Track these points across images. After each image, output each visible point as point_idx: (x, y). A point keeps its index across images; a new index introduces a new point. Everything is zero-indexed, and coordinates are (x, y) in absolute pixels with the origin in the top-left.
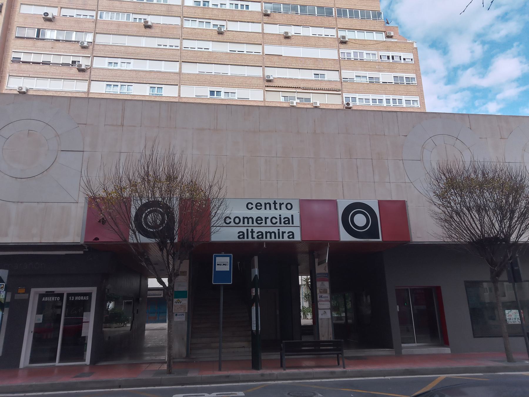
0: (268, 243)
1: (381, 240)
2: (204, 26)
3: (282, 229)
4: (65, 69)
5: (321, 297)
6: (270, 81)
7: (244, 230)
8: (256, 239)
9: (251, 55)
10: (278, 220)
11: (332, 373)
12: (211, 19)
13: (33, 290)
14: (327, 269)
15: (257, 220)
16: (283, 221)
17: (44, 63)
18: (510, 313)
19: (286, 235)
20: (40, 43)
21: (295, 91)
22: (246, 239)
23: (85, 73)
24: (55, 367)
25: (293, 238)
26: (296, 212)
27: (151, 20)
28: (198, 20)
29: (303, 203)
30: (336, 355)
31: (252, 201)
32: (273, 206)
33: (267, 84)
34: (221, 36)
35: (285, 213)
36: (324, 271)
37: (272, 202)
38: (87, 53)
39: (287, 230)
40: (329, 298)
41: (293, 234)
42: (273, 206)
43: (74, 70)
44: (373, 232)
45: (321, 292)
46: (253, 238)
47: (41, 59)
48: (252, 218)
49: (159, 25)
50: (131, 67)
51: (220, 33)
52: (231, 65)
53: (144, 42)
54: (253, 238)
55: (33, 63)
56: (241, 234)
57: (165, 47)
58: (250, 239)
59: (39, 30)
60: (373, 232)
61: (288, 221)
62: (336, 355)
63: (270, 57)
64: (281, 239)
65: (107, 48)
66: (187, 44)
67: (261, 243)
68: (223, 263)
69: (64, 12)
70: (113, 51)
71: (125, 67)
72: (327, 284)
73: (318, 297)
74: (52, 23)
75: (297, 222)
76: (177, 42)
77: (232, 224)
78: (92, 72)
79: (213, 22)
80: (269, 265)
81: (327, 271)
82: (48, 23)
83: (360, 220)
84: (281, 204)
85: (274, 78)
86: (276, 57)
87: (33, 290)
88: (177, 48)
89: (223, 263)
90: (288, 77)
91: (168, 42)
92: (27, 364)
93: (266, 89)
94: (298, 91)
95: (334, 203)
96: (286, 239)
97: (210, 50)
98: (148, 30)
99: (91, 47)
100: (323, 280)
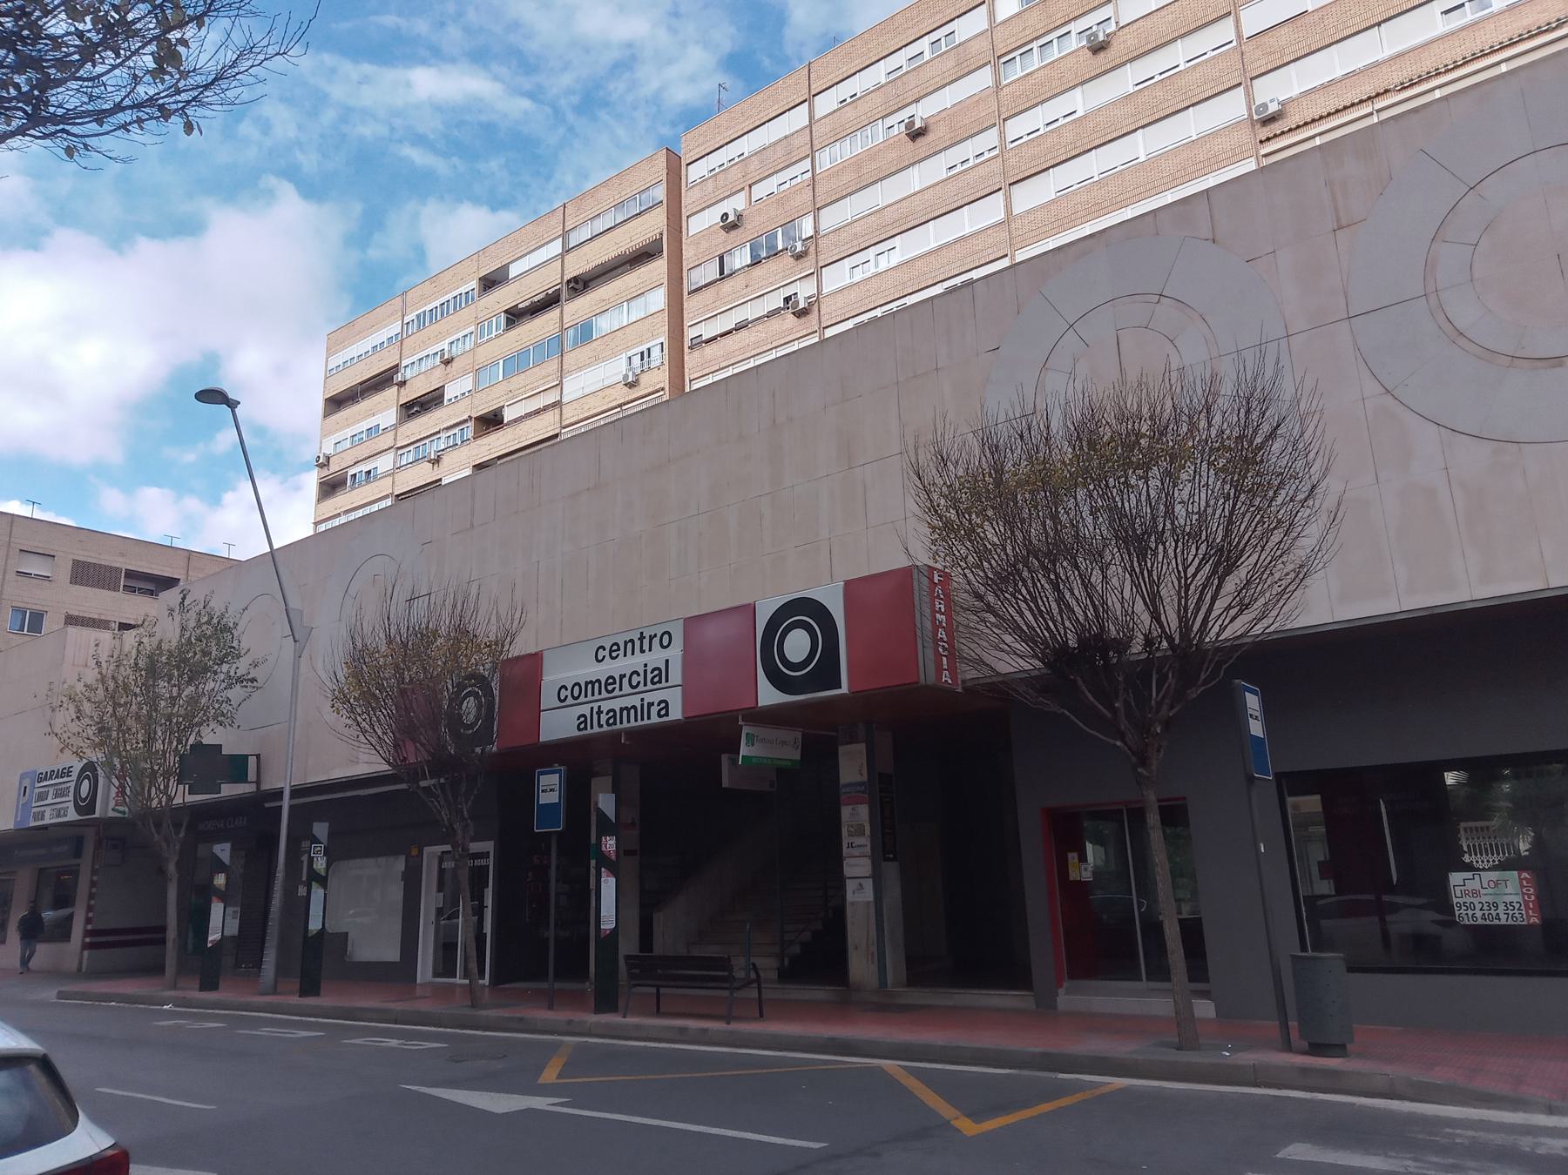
0: (630, 733)
1: (844, 689)
2: (1055, 53)
3: (649, 698)
4: (775, 324)
5: (850, 845)
6: (1272, 119)
7: (585, 710)
8: (605, 728)
9: (1206, 61)
10: (641, 679)
11: (683, 1030)
12: (1069, 22)
13: (427, 850)
14: (865, 772)
15: (607, 684)
16: (649, 676)
17: (739, 327)
18: (1470, 885)
19: (654, 710)
20: (727, 286)
21: (1369, 110)
22: (589, 731)
23: (809, 317)
24: (455, 985)
25: (667, 714)
26: (675, 653)
27: (922, 111)
28: (1035, 45)
29: (691, 623)
30: (654, 990)
31: (602, 646)
32: (637, 643)
33: (1264, 133)
34: (1102, 55)
35: (656, 657)
36: (859, 779)
37: (636, 637)
38: (808, 266)
39: (655, 697)
40: (868, 850)
41: (667, 707)
42: (637, 643)
43: (790, 318)
44: (825, 672)
45: (850, 835)
46: (600, 726)
47: (728, 322)
48: (599, 681)
49: (944, 115)
50: (895, 259)
51: (1098, 48)
52: (1143, 127)
53: (932, 171)
54: (600, 726)
55: (722, 335)
56: (583, 721)
57: (966, 166)
58: (596, 729)
59: (721, 258)
60: (825, 672)
61: (659, 676)
62: (654, 990)
63: (1265, 39)
64: (646, 722)
65: (844, 235)
66: (1018, 128)
67: (618, 733)
68: (550, 788)
69: (760, 191)
70: (856, 236)
71: (884, 264)
72: (864, 811)
73: (845, 846)
74: (740, 230)
75: (676, 675)
76: (990, 138)
77: (570, 701)
78: (823, 307)
79: (1076, 27)
80: (673, 779)
81: (865, 778)
82: (733, 233)
83: (797, 645)
84: (651, 638)
85: (1282, 104)
86: (1285, 30)
87: (427, 850)
88: (993, 153)
89: (550, 788)
90: (1338, 73)
91: (968, 149)
92: (429, 977)
93: (1263, 152)
94: (1377, 106)
95: (751, 610)
96: (655, 719)
97: (1079, 114)
98: (921, 141)
99: (812, 250)
100: (855, 801)
